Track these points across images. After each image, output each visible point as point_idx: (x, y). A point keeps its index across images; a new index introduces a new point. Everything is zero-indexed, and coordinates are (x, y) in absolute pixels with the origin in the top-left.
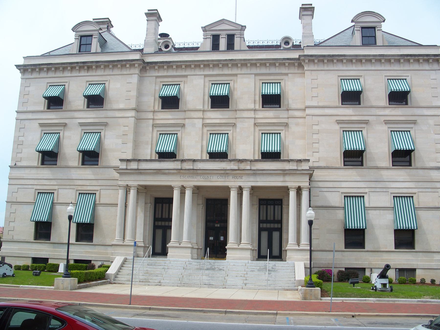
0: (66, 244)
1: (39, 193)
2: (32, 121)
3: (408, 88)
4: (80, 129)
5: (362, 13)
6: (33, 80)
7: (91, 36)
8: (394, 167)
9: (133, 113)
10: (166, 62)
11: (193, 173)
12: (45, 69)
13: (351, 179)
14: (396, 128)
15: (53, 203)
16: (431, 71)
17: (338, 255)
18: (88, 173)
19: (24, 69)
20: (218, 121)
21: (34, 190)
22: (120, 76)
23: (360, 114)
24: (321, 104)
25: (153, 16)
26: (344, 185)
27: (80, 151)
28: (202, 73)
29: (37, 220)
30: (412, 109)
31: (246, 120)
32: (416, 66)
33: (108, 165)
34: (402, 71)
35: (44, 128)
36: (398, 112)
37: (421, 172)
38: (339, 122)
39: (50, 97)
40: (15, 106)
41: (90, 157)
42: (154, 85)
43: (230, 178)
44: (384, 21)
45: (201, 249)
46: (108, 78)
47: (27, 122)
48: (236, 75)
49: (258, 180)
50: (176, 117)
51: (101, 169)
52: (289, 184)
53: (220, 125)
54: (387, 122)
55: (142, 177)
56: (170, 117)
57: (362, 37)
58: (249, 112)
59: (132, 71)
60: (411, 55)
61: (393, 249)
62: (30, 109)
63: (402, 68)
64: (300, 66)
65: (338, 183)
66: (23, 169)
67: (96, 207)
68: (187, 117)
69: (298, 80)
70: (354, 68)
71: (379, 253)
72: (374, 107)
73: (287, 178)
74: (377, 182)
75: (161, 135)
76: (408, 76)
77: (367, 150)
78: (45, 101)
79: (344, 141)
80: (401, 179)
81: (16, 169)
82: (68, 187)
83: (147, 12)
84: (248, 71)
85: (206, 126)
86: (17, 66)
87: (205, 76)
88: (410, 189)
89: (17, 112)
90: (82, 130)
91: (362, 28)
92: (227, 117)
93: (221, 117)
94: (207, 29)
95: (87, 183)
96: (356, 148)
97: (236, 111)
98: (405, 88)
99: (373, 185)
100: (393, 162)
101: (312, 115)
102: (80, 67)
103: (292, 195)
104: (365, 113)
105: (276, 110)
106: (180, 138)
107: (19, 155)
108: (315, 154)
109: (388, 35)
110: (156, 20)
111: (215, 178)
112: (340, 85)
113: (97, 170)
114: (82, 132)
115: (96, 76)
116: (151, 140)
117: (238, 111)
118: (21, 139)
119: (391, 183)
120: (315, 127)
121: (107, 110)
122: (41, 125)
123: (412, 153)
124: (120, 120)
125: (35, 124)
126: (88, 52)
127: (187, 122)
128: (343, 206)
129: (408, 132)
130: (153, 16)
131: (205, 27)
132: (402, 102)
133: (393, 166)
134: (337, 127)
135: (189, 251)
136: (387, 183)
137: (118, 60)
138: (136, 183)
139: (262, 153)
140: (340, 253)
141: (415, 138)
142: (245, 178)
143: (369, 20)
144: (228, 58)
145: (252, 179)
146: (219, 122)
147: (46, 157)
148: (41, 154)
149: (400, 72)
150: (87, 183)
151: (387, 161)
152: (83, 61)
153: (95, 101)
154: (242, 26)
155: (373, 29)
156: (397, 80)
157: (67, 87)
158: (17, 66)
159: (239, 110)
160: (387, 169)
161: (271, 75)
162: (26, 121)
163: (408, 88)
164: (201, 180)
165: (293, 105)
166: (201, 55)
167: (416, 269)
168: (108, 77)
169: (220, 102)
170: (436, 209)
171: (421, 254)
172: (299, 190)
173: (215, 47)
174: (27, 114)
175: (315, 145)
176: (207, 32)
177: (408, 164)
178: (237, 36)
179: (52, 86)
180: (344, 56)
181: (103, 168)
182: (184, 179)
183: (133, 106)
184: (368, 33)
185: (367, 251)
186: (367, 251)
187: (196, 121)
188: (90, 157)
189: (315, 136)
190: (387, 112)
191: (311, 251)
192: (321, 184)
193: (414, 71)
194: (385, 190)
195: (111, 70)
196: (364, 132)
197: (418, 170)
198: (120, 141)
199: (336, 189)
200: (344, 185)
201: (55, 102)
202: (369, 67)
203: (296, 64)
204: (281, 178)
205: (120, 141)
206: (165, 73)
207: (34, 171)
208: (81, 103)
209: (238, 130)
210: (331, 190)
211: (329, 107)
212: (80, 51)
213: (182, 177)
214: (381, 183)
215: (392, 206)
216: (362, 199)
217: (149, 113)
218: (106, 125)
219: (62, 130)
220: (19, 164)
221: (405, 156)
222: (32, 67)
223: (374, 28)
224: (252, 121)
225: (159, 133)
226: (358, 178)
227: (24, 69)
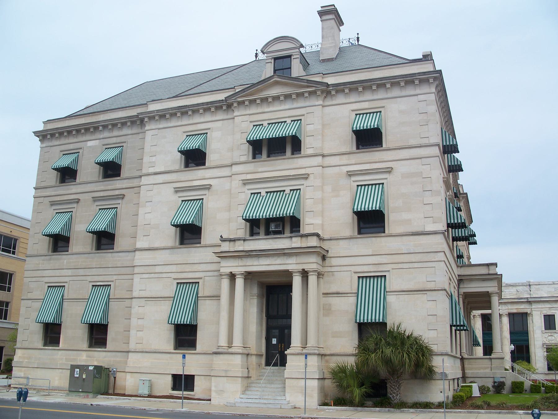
19: (42, 135)
25: (330, 14)
27: (176, 226)
29: (176, 323)
39: (254, 141)
41: (370, 221)
45: (184, 357)
54: (177, 190)
57: (290, 68)
75: (360, 187)
83: (320, 9)
86: (37, 134)
89: (35, 188)
103: (297, 281)
109: (373, 51)
110: (334, 19)
125: (168, 190)
130: (330, 14)
143: (282, 48)
147: (187, 235)
148: (95, 236)
153: (111, 170)
158: (37, 134)
172: (305, 274)
188: (104, 239)
201: (67, 174)
202: (396, 92)
222: (204, 106)
227: (42, 135)
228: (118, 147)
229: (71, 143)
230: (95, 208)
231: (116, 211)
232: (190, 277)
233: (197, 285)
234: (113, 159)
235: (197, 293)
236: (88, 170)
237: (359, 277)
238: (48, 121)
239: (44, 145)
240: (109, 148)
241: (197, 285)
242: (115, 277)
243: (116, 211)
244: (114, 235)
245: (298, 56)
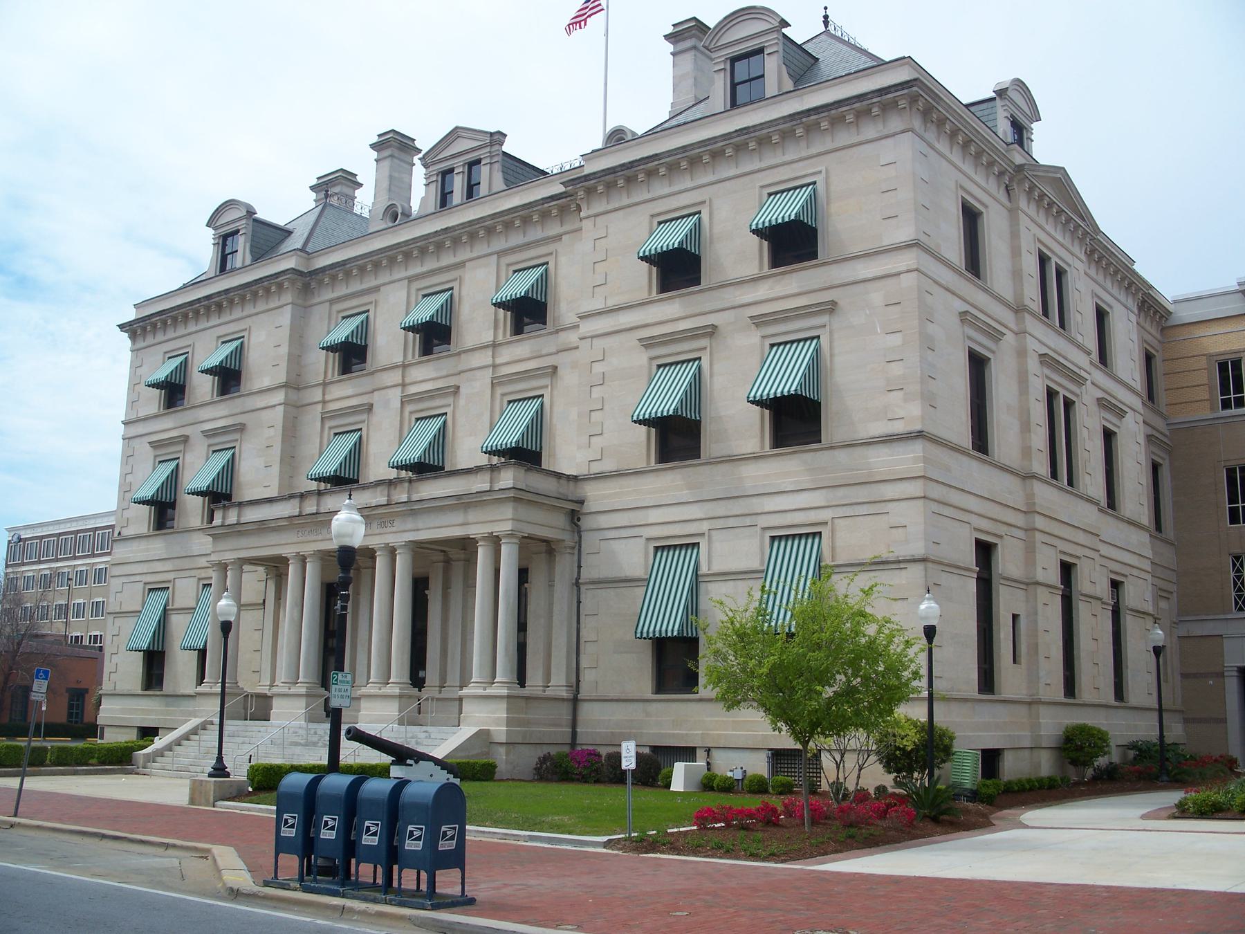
0: (939, 699)
1: (657, 548)
4: (207, 442)
5: (725, 18)
7: (760, 51)
12: (554, 212)
13: (671, 499)
15: (165, 610)
16: (883, 141)
18: (792, 467)
19: (134, 329)
21: (141, 585)
23: (698, 311)
26: (654, 516)
28: (403, 274)
30: (827, 268)
32: (844, 137)
34: (806, 162)
35: (213, 441)
37: (841, 456)
40: (121, 414)
41: (795, 419)
42: (326, 322)
48: (461, 265)
49: (420, 525)
52: (473, 531)
54: (759, 321)
55: (243, 542)
57: (763, 76)
59: (895, 123)
60: (817, 110)
61: (649, 695)
63: (804, 154)
65: (640, 513)
67: (702, 587)
72: (730, 285)
73: (472, 516)
74: (731, 501)
76: (820, 172)
78: (406, 337)
80: (788, 485)
87: (500, 254)
88: (812, 513)
90: (763, 337)
93: (434, 375)
99: (720, 509)
101: (592, 337)
105: (535, 337)
106: (364, 438)
108: (594, 439)
114: (650, 364)
115: (789, 163)
119: (882, 487)
126: (758, 99)
127: (561, 360)
135: (302, 702)
136: (754, 500)
140: (641, 705)
141: (832, 356)
145: (410, 524)
149: (801, 164)
152: (878, 87)
153: (792, 243)
154: (492, 134)
157: (820, 187)
160: (755, 458)
167: (157, 729)
170: (881, 567)
175: (596, 416)
179: (776, 193)
180: (655, 157)
182: (304, 539)
183: (282, 378)
186: (701, 700)
188: (795, 419)
191: (1160, 710)
192: (604, 521)
193: (838, 154)
194: (748, 521)
195: (853, 130)
197: (836, 452)
199: (637, 529)
200: (654, 516)
204: (457, 517)
207: (143, 545)
208: (754, 253)
209: (462, 401)
210: (624, 533)
212: (734, 104)
214: (740, 500)
226: (685, 495)
227: (134, 329)
228: (689, 215)
229: (176, 339)
230: (752, 339)
231: (699, 368)
232: (776, 524)
233: (817, 540)
234: (681, 243)
235: (697, 568)
236: (734, 251)
237: (657, 548)
238: (594, 151)
239: (140, 344)
240: (666, 222)
241: (817, 540)
242: (704, 527)
243: (699, 368)
244: (697, 424)
245: (780, 48)
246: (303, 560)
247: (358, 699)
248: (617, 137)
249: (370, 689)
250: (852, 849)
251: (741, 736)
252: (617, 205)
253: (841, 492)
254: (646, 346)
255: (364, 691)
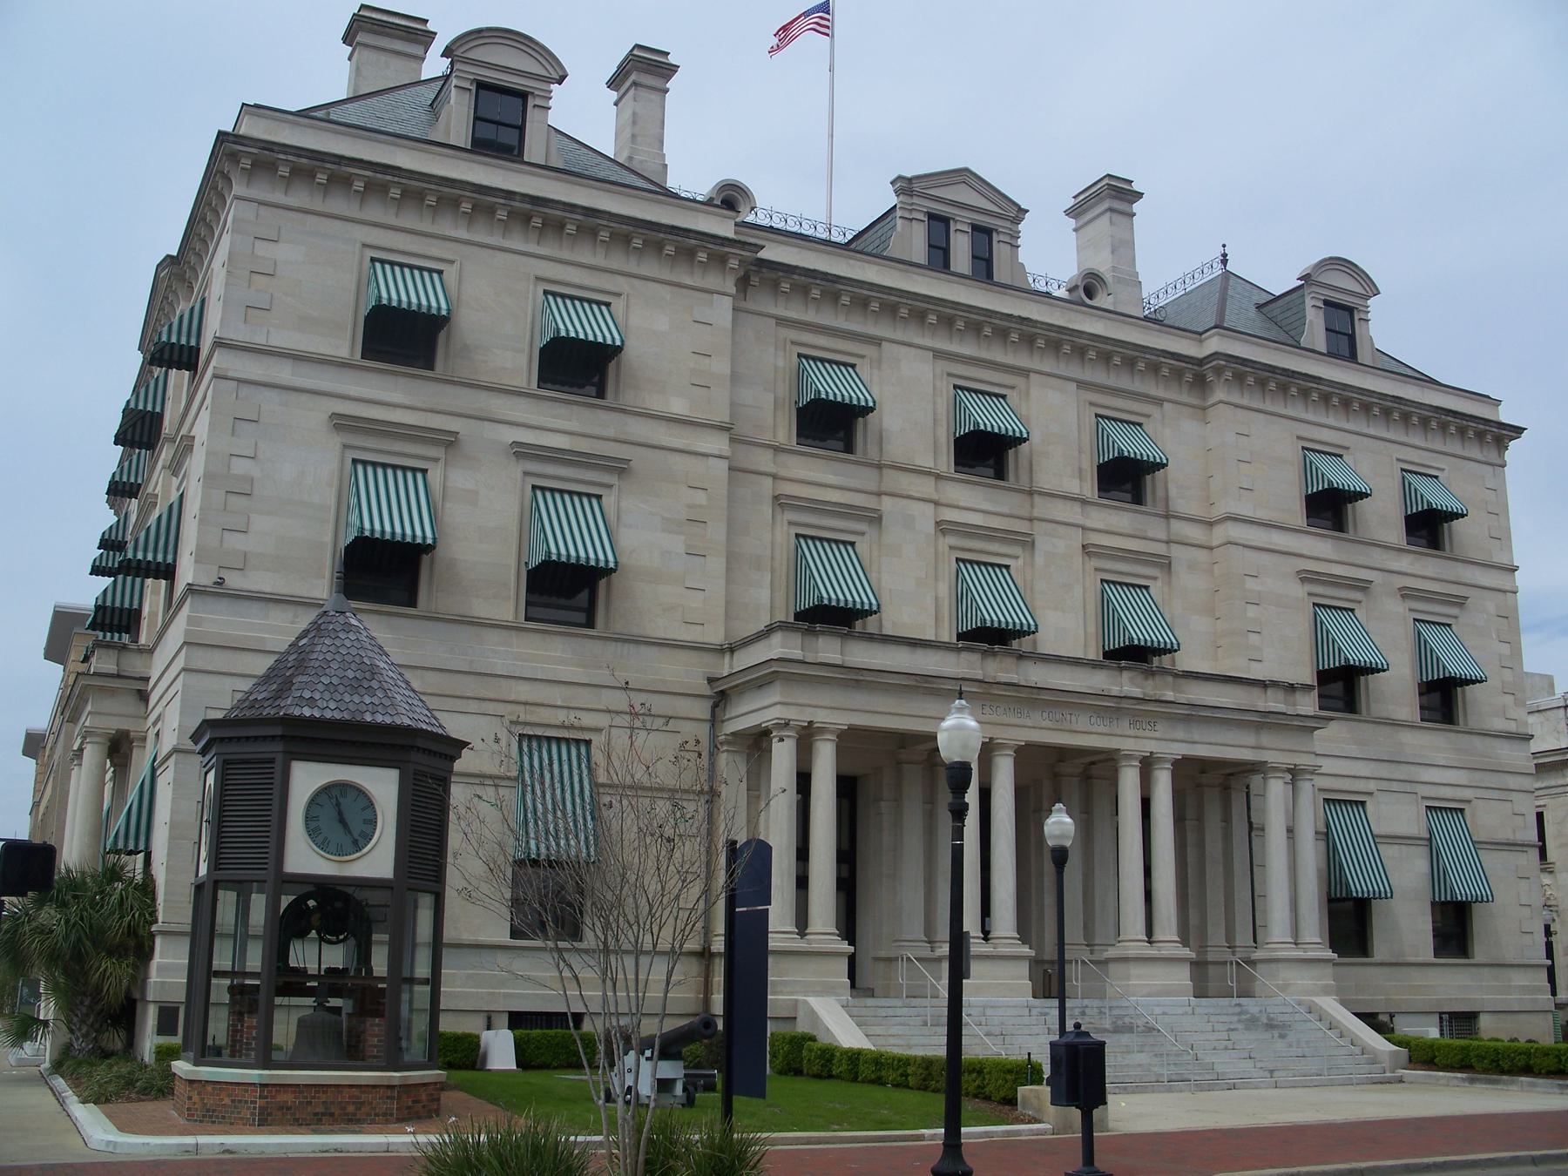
2: (293, 396)
3: (444, 305)
4: (516, 469)
6: (291, 214)
8: (532, 625)
9: (717, 444)
10: (825, 276)
11: (1019, 700)
14: (555, 477)
17: (1418, 978)
18: (1433, 743)
20: (977, 519)
22: (668, 288)
23: (588, 431)
24: (1261, 514)
31: (1062, 530)
33: (635, 631)
36: (563, 422)
37: (1477, 742)
38: (1306, 577)
41: (565, 591)
43: (1124, 726)
44: (560, 81)
46: (621, 284)
47: (270, 402)
49: (1197, 737)
50: (853, 483)
51: (612, 647)
53: (988, 534)
54: (1406, 594)
55: (860, 699)
56: (830, 479)
57: (476, 118)
58: (1069, 503)
59: (713, 280)
61: (1431, 958)
62: (278, 340)
64: (1200, 383)
66: (256, 607)
68: (888, 490)
69: (1189, 426)
70: (1331, 421)
71: (1405, 969)
73: (1266, 739)
77: (440, 552)
79: (353, 500)
81: (224, 604)
82: (473, 706)
84: (1062, 369)
85: (944, 532)
91: (482, 86)
92: (1005, 510)
94: (916, 186)
95: (556, 695)
96: (393, 533)
97: (1031, 493)
98: (394, 296)
100: (528, 603)
102: (406, 193)
104: (1361, 560)
107: (235, 542)
111: (1082, 721)
112: (365, 281)
113: (596, 647)
116: (768, 552)
117: (885, 471)
118: (240, 467)
119: (1421, 769)
120: (1250, 584)
121: (623, 411)
122: (341, 423)
123: (602, 583)
124: (679, 463)
128: (514, 773)
129: (419, 476)
131: (910, 180)
132: (582, 386)
133: (527, 619)
134: (1299, 591)
136: (1412, 768)
137: (673, 227)
138: (844, 720)
139: (1320, 673)
142: (1162, 729)
144: (1016, 313)
146: (842, 501)
150: (556, 695)
151: (507, 603)
155: (520, 101)
156: (426, 274)
159: (1041, 493)
161: (1118, 396)
162: (267, 392)
163: (444, 305)
164: (1044, 724)
165: (1180, 505)
166: (920, 279)
168: (621, 280)
169: (984, 453)
171: (1486, 970)
173: (939, 257)
174: (266, 359)
175: (1253, 638)
176: (915, 200)
177: (582, 617)
178: (1002, 238)
180: (1318, 380)
181: (616, 640)
184: (501, 108)
185: (1381, 964)
186: (1381, 964)
187: (916, 508)
189: (1252, 611)
190: (1404, 563)
194: (1408, 787)
196: (435, 475)
198: (677, 544)
203: (1189, 377)
204: (1248, 738)
205: (677, 544)
206: (811, 316)
209: (1039, 559)
211: (1252, 522)
213: (987, 709)
215: (514, 773)
216: (583, 750)
217: (760, 450)
218: (620, 468)
219: (436, 460)
220: (234, 581)
221: (571, 593)
223: (523, 96)
224: (1077, 538)
225: (794, 530)
246: (806, 738)
247: (1107, 961)
248: (730, 198)
249: (1134, 950)
250: (216, 1127)
251: (1513, 1000)
252: (408, 225)
253: (1478, 775)
254: (1303, 580)
255: (1111, 953)
